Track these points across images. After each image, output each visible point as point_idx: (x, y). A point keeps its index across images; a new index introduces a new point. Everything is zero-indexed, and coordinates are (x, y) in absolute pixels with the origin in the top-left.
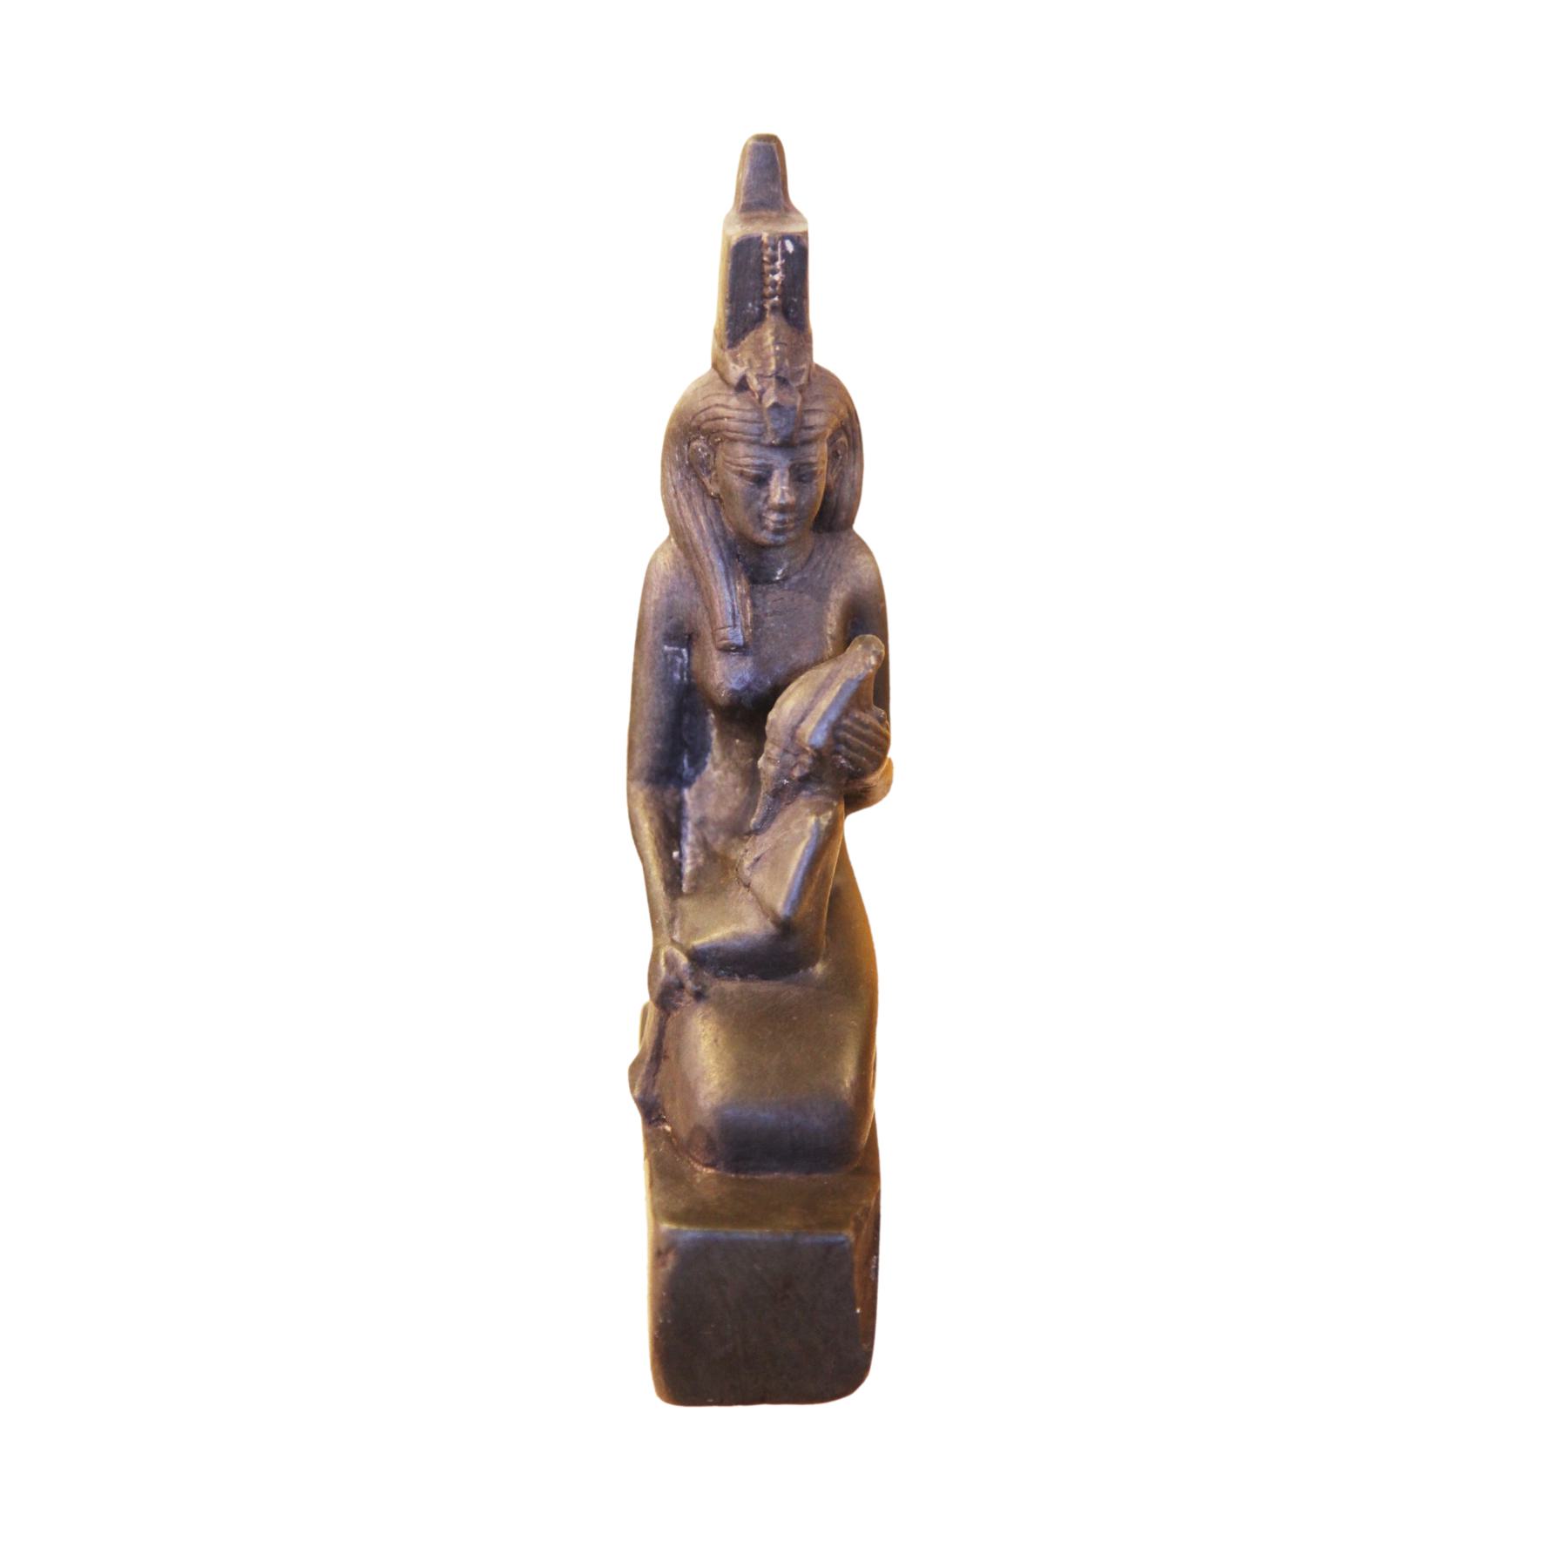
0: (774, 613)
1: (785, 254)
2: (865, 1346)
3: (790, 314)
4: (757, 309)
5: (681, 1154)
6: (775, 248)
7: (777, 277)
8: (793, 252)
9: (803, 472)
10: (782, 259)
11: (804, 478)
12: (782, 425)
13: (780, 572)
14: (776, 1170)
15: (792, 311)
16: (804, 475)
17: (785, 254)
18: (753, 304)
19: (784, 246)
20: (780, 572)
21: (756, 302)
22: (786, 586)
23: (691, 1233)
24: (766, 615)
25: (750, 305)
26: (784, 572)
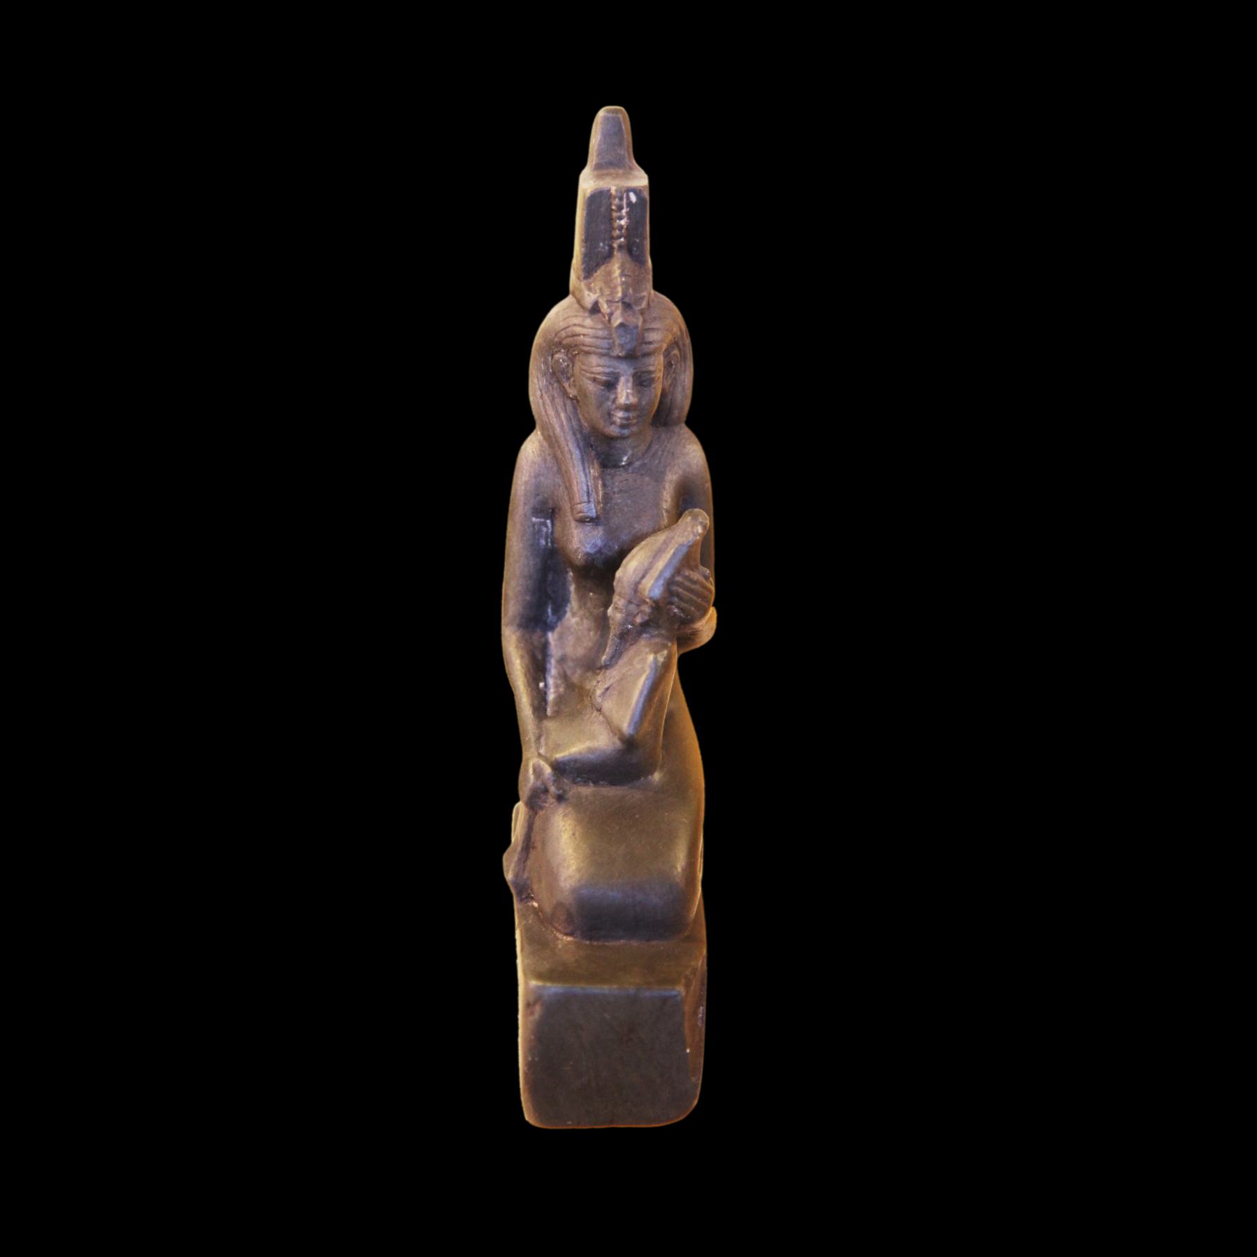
0: (621, 491)
1: (630, 204)
3: (634, 252)
4: (607, 248)
5: (546, 925)
6: (621, 199)
7: (623, 222)
8: (636, 202)
9: (644, 379)
10: (627, 208)
11: (645, 384)
12: (627, 341)
13: (625, 459)
14: (622, 938)
15: (635, 249)
16: (644, 381)
17: (630, 204)
18: (604, 244)
19: (628, 197)
20: (625, 459)
21: (606, 242)
22: (630, 470)
24: (614, 493)
25: (601, 244)
26: (628, 458)
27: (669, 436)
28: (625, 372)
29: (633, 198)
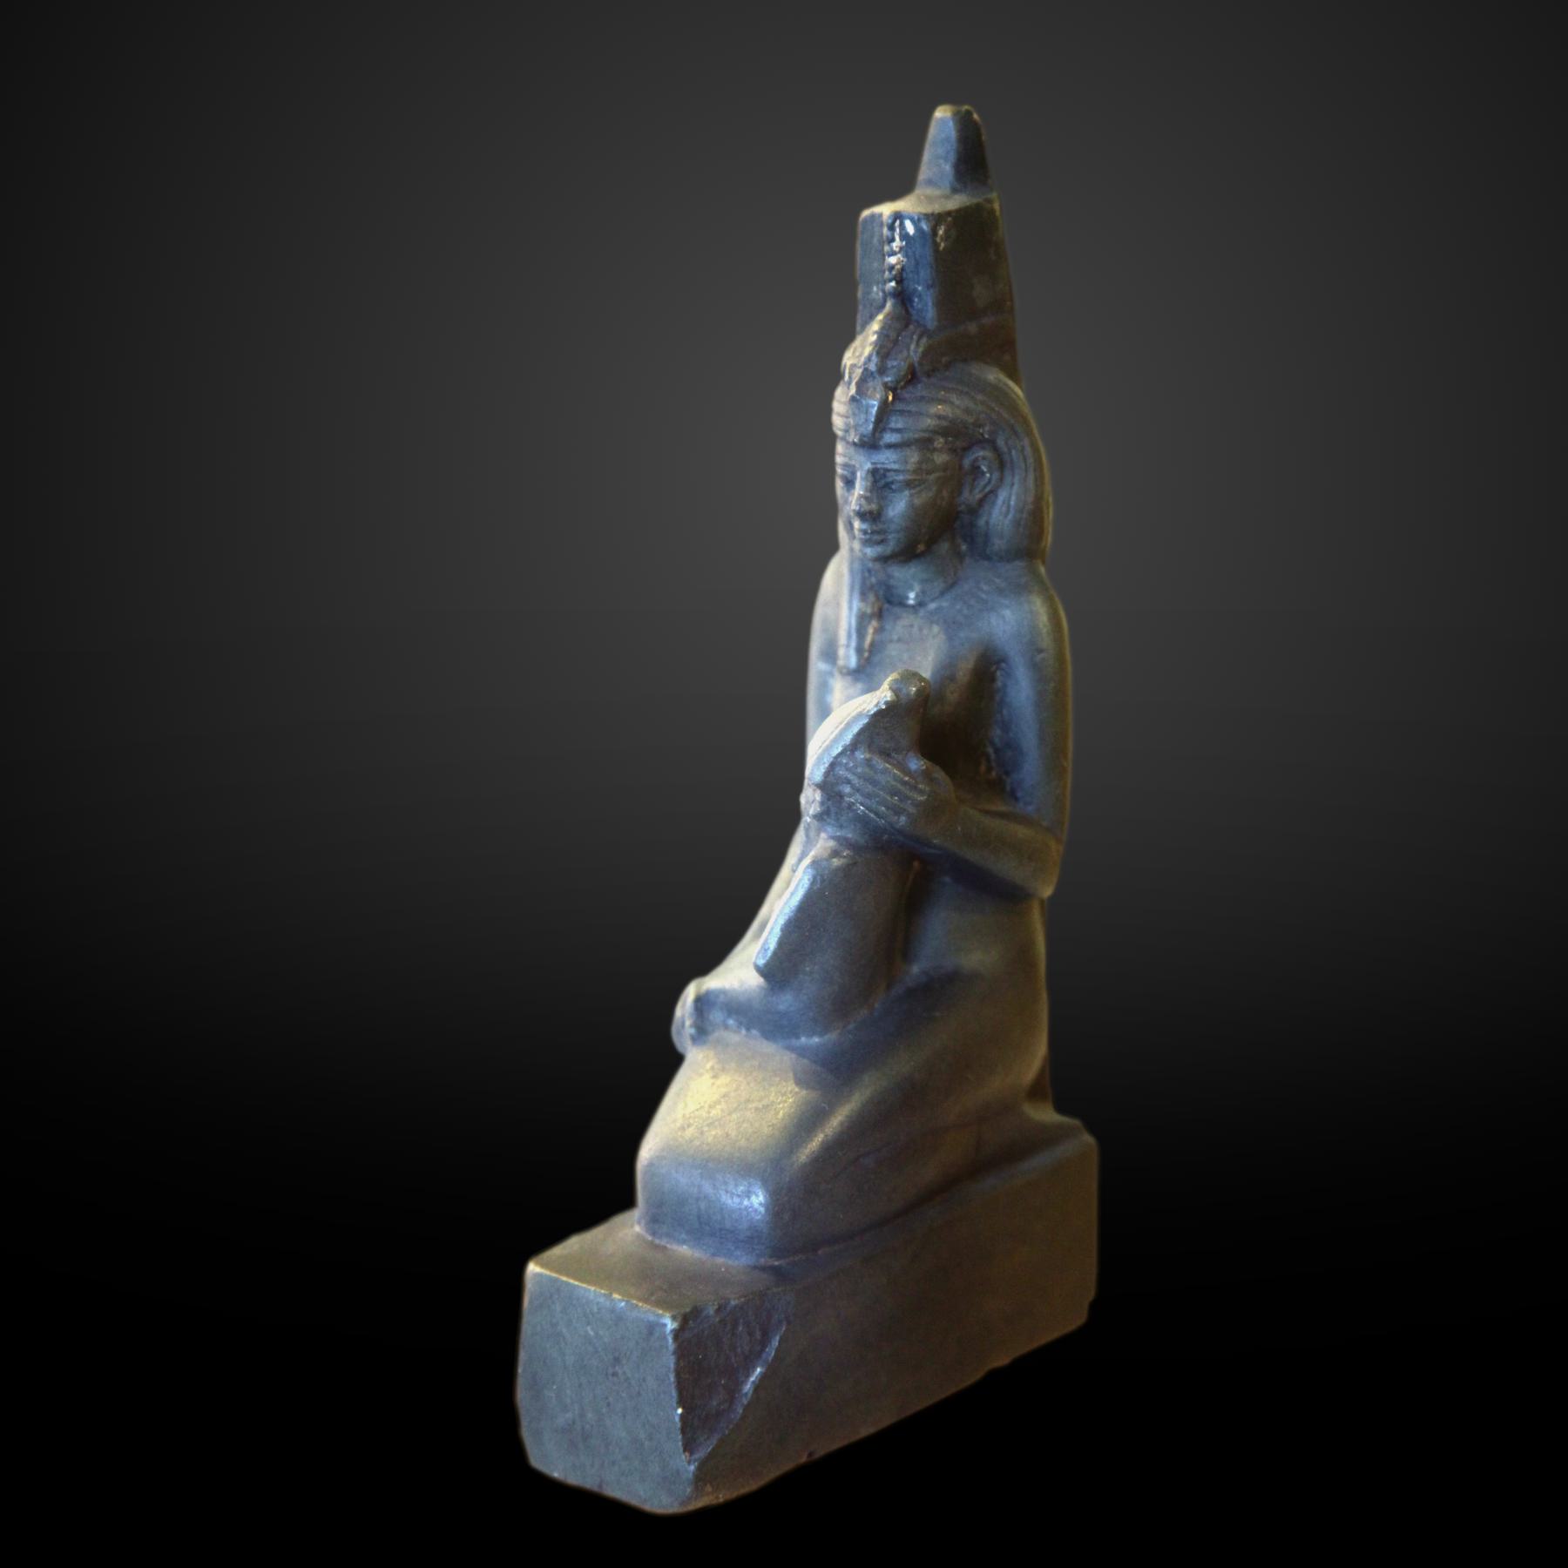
0: (899, 640)
1: (904, 236)
3: (915, 304)
4: (881, 294)
5: (745, 1213)
6: (891, 228)
7: (893, 260)
8: (914, 234)
9: (890, 480)
10: (901, 240)
11: (893, 487)
12: (860, 423)
13: (912, 595)
14: (684, 1242)
15: (916, 300)
16: (892, 483)
17: (904, 236)
18: (878, 288)
19: (902, 226)
20: (912, 595)
21: (880, 285)
22: (922, 612)
24: (891, 641)
25: (875, 289)
26: (917, 596)
28: (861, 466)
29: (910, 228)
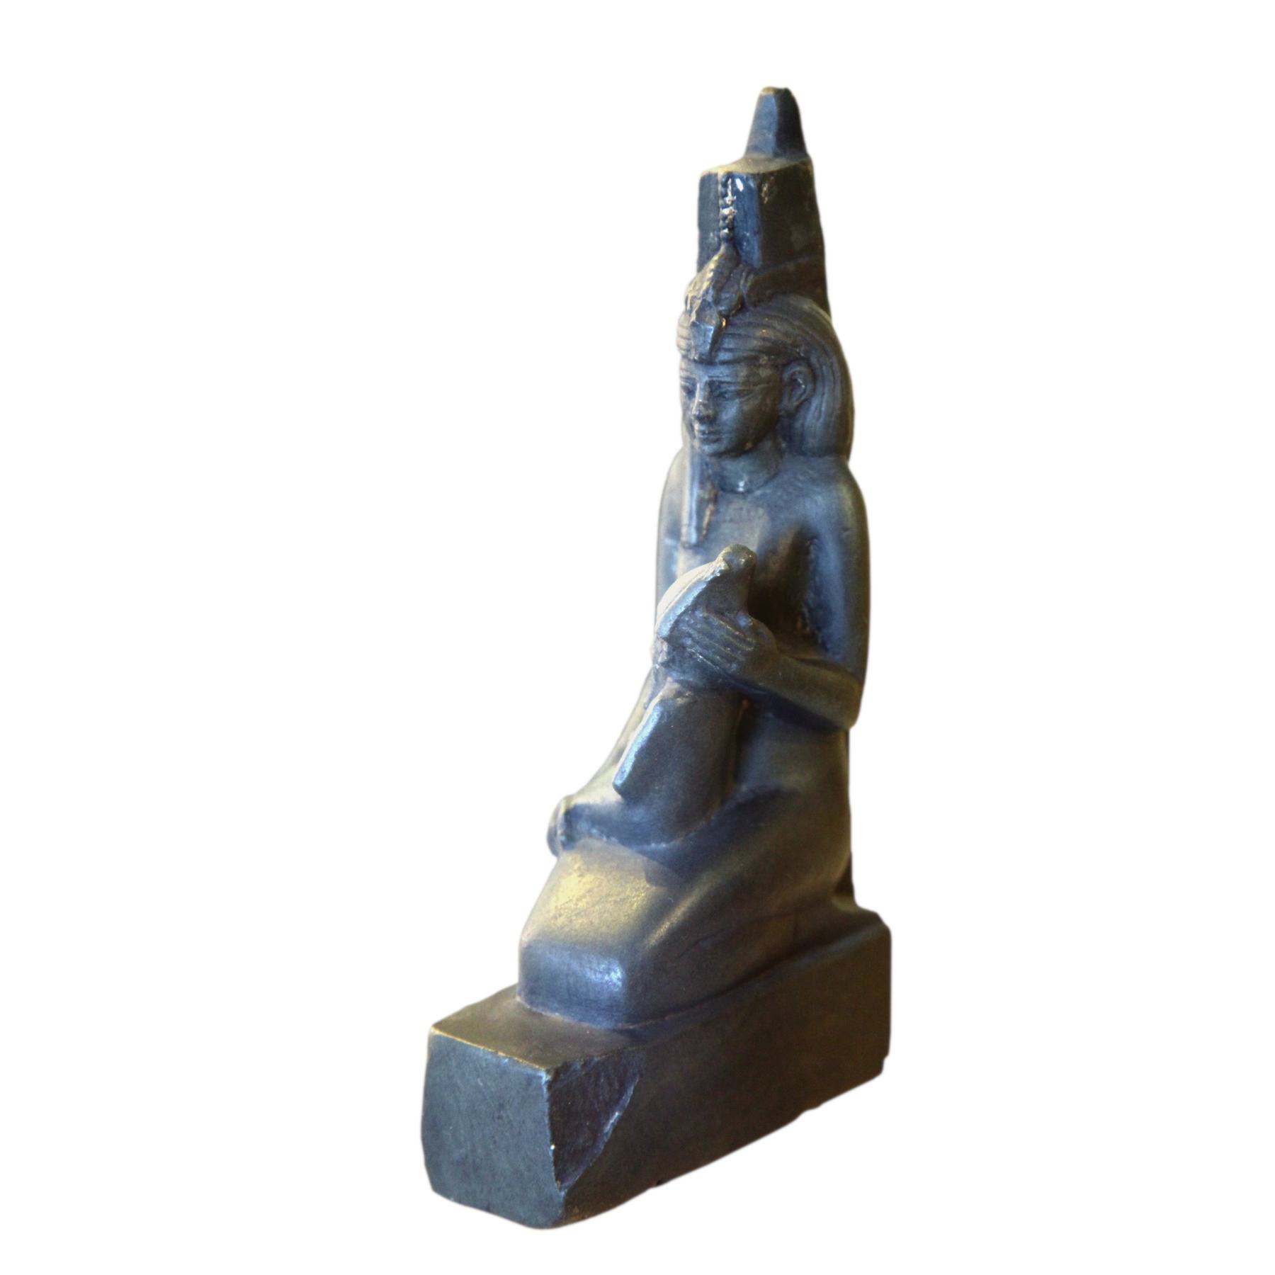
0: (731, 521)
1: (735, 192)
2: (586, 1216)
3: (744, 247)
4: (716, 239)
5: (606, 986)
6: (725, 185)
7: (726, 211)
8: (743, 191)
9: (724, 390)
10: (733, 195)
11: (726, 396)
12: (700, 344)
13: (742, 484)
14: (556, 1010)
15: (745, 244)
16: (725, 393)
17: (735, 192)
18: (714, 234)
19: (734, 184)
20: (742, 484)
21: (716, 232)
22: (750, 498)
23: (438, 1032)
24: (725, 521)
25: (711, 235)
26: (746, 485)
27: (832, 472)
29: (740, 185)
